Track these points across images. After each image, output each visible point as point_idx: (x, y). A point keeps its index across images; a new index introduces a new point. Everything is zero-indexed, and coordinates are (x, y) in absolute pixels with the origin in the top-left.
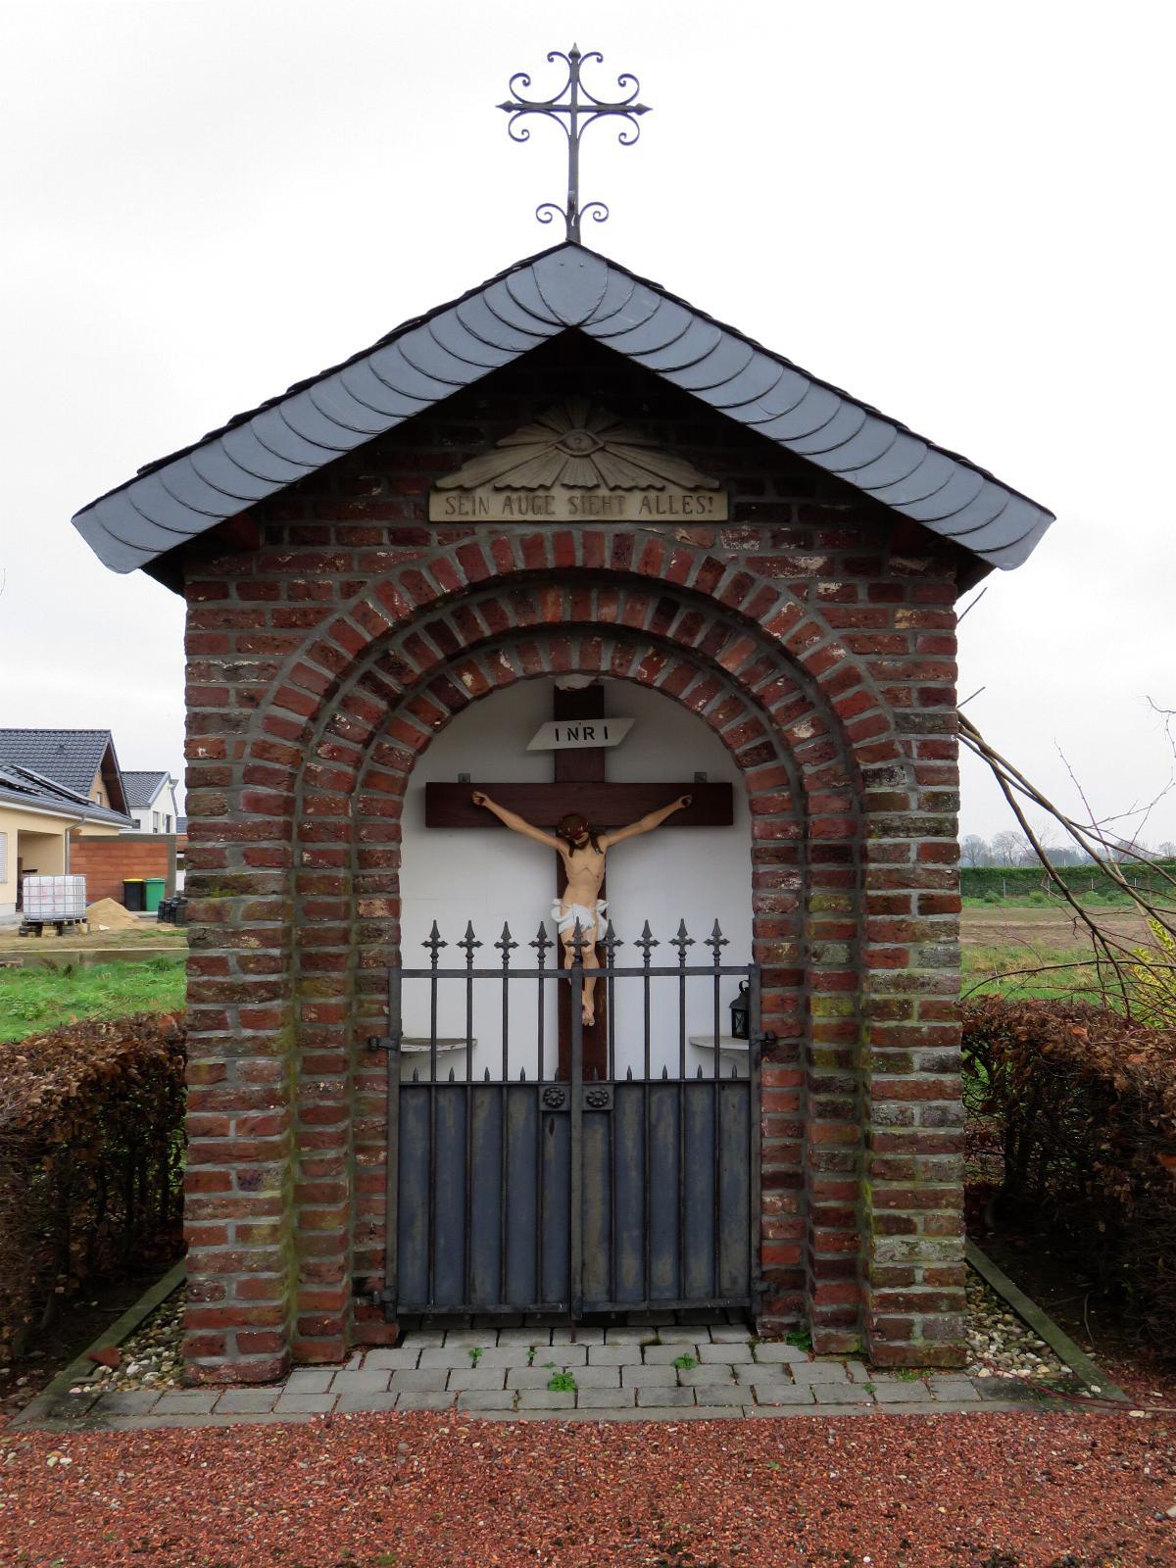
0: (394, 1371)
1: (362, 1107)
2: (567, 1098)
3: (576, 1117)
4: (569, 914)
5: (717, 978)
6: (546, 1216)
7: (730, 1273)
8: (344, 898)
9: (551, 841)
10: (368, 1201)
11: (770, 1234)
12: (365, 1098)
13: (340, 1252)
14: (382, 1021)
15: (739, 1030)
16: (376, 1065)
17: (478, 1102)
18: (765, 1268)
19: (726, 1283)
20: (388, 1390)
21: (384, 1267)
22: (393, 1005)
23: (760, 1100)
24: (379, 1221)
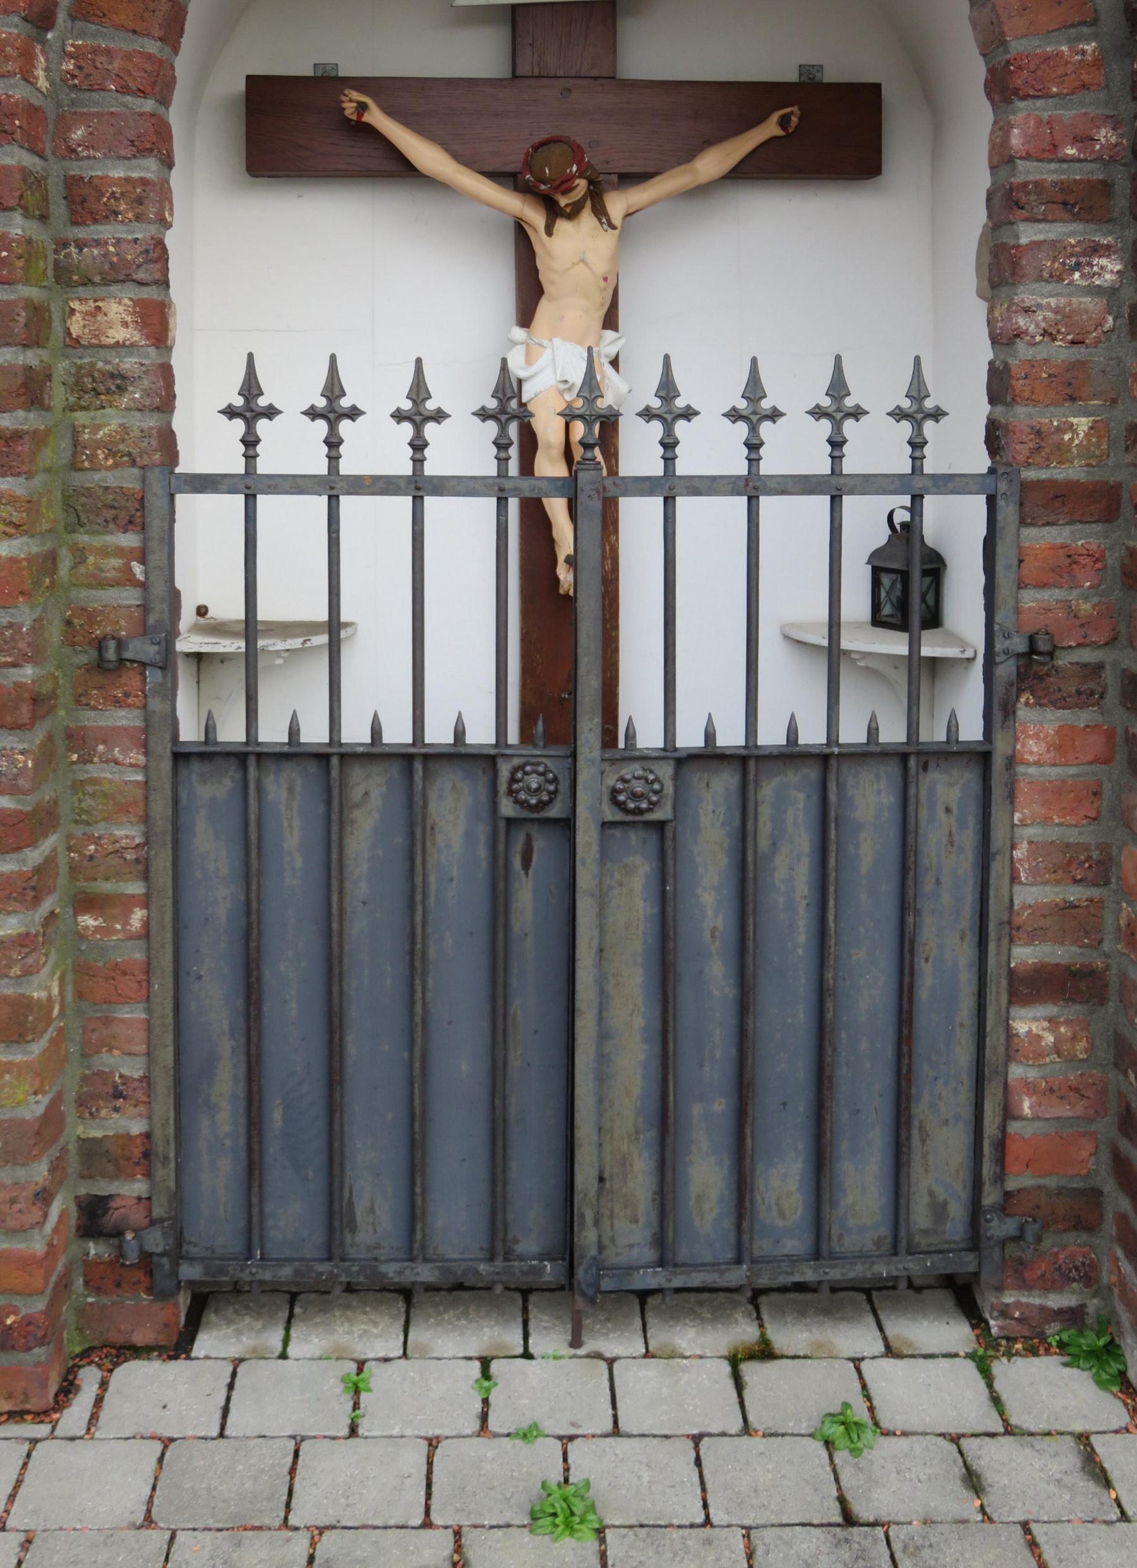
0: (167, 1442)
1: (89, 802)
2: (564, 786)
3: (587, 836)
4: (545, 358)
5: (669, 502)
6: (514, 1063)
7: (932, 1194)
8: (32, 293)
9: (512, 202)
10: (107, 1021)
11: (1026, 1106)
12: (94, 781)
13: (36, 1158)
14: (130, 597)
15: (887, 610)
16: (118, 703)
17: (356, 793)
18: (1011, 1185)
19: (920, 1216)
20: (149, 1521)
21: (148, 1175)
22: (155, 559)
23: (1011, 797)
24: (134, 1069)
